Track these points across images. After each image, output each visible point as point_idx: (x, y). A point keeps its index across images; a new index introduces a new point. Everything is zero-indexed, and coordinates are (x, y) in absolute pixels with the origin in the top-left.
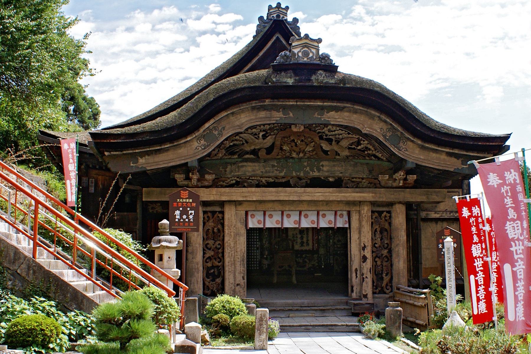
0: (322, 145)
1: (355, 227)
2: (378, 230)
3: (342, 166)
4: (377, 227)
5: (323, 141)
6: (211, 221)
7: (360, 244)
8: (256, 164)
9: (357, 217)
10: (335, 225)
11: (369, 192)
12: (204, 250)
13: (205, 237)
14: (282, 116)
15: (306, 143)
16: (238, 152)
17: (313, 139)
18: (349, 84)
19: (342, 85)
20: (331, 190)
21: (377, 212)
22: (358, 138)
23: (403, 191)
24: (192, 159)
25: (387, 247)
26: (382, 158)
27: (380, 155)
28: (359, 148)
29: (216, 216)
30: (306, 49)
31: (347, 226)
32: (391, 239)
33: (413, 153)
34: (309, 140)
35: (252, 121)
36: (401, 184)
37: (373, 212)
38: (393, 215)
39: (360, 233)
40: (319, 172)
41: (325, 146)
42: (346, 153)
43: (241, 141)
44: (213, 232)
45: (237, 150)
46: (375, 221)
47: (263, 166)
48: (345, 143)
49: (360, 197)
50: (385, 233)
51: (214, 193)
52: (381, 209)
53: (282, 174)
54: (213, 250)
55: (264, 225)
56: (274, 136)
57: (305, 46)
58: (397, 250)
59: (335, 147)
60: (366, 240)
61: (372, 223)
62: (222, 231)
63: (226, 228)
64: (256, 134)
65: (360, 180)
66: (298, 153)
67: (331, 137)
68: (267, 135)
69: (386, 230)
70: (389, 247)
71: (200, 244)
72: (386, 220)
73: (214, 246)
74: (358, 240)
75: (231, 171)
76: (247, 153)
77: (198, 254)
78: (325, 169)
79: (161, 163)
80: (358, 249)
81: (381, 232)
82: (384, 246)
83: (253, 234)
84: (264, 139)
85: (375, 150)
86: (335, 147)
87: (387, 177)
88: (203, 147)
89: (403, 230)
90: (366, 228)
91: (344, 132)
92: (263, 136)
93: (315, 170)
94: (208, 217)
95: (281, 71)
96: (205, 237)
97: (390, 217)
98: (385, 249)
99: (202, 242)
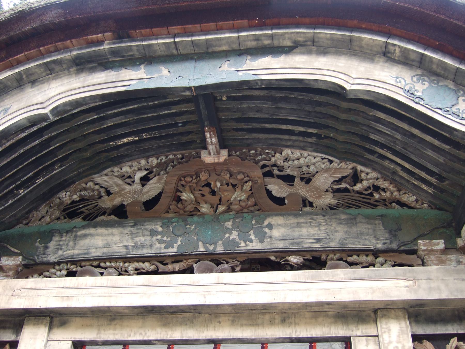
0: (271, 187)
3: (319, 225)
5: (272, 180)
8: (115, 231)
11: (397, 278)
16: (82, 212)
21: (431, 338)
34: (240, 176)
40: (262, 241)
41: (277, 189)
42: (329, 199)
45: (83, 209)
47: (132, 233)
48: (323, 181)
53: (173, 250)
59: (300, 189)
64: (130, 177)
65: (370, 259)
68: (151, 176)
75: (59, 248)
78: (276, 233)
84: (143, 185)
86: (300, 189)
87: (440, 244)
92: (142, 179)
93: (252, 237)
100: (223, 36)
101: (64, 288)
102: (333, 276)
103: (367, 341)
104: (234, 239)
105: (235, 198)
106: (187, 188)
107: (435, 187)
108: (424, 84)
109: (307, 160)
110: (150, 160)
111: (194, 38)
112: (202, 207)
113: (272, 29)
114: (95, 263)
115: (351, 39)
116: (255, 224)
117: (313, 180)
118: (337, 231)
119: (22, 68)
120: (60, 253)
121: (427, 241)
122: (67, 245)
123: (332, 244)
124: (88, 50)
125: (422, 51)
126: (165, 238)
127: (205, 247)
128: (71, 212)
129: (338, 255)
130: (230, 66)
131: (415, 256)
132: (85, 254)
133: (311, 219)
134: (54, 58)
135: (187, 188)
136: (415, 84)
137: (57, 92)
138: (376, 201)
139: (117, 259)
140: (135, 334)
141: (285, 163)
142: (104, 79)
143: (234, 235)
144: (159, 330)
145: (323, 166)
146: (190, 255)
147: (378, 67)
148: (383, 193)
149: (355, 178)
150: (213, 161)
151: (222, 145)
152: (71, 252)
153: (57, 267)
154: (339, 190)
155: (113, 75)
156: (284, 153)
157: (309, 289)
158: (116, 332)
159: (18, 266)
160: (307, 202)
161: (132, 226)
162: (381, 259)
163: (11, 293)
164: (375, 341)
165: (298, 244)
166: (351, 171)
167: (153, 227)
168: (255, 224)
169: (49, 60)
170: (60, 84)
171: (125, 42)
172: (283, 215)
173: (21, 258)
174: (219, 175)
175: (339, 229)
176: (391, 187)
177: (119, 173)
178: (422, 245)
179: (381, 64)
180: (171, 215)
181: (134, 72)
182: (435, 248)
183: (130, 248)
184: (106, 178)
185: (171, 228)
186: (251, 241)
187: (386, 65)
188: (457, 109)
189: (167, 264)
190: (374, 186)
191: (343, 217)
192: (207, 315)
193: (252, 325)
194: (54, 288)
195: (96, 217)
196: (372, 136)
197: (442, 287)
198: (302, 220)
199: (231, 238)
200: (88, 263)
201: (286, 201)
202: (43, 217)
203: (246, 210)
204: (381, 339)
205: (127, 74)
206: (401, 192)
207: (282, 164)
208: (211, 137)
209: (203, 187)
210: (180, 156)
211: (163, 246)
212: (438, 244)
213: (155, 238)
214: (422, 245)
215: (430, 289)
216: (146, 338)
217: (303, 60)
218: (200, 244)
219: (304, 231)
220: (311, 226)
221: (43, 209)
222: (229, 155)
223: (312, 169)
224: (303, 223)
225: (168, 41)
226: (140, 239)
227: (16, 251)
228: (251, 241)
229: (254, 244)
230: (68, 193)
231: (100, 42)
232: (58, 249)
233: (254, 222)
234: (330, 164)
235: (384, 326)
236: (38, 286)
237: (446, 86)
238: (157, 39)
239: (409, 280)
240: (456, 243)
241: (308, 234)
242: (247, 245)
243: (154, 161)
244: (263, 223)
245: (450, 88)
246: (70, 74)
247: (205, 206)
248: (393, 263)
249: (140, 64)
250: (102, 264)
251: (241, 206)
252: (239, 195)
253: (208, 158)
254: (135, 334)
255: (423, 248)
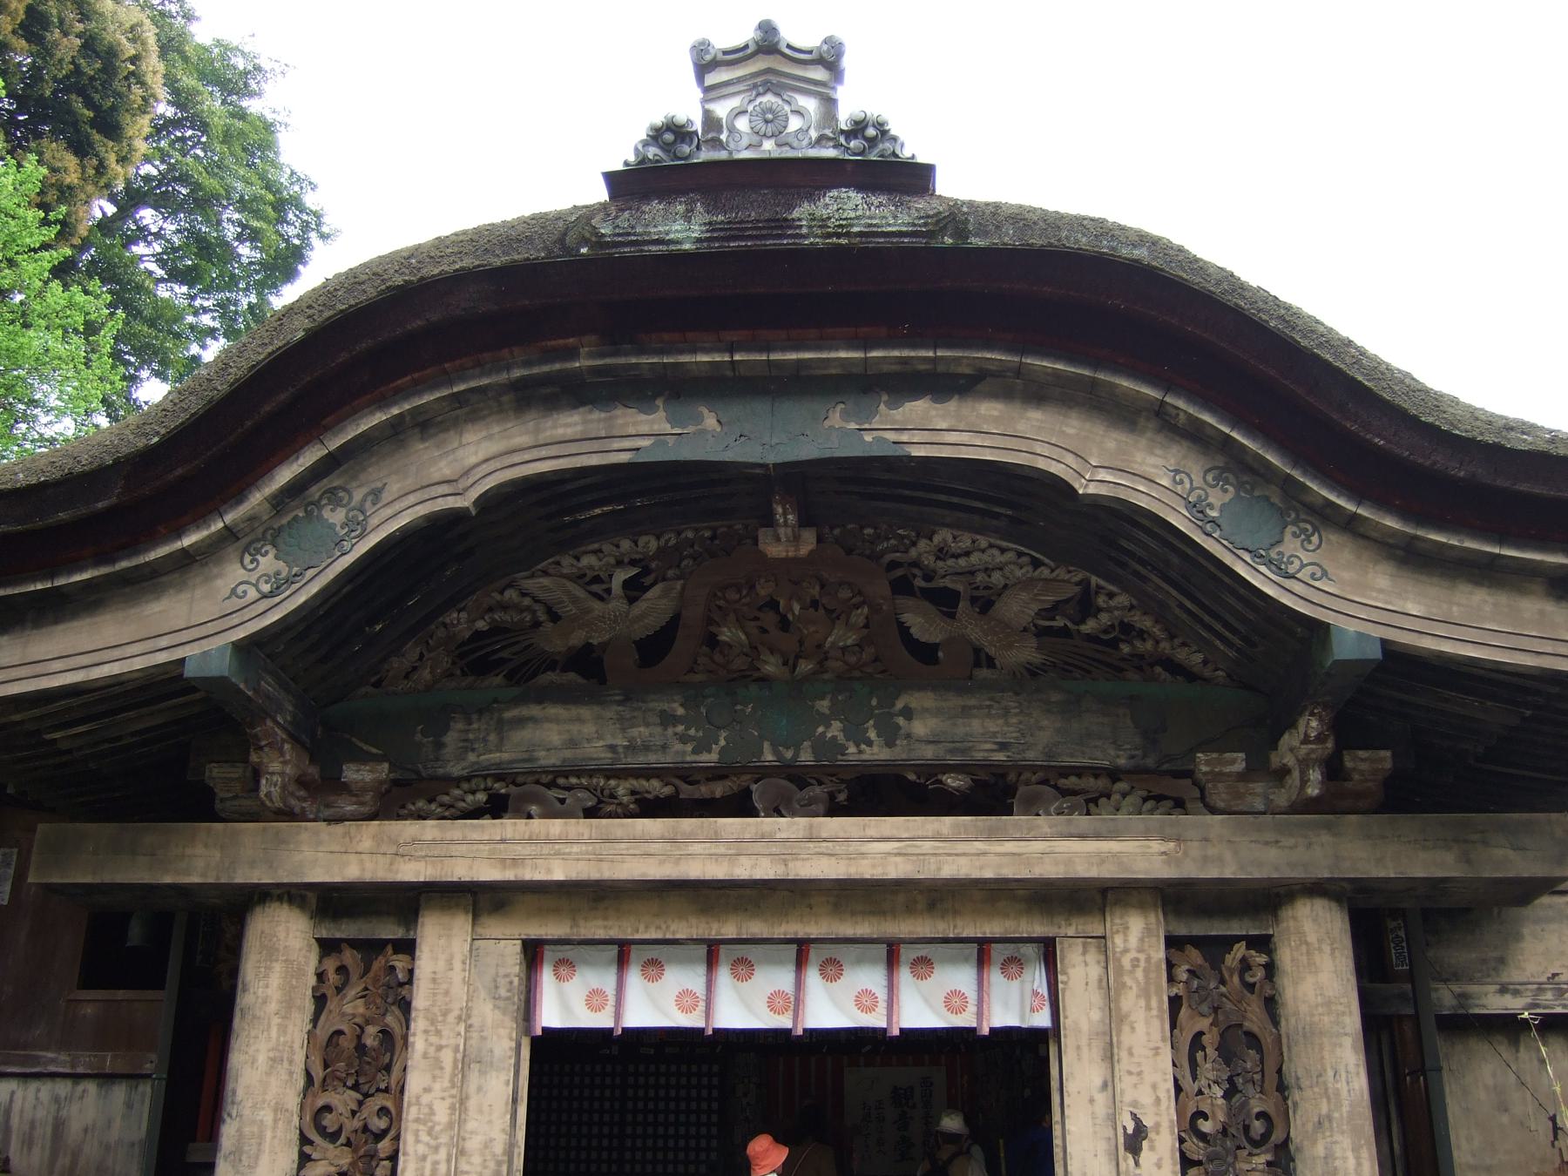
0: (909, 618)
1: (1085, 1026)
2: (1210, 1040)
3: (1006, 713)
4: (1204, 1024)
5: (910, 602)
6: (352, 992)
7: (1113, 1119)
8: (585, 712)
9: (1095, 971)
10: (980, 1015)
11: (1146, 835)
12: (304, 1140)
13: (318, 1073)
14: (667, 428)
15: (829, 611)
16: (503, 661)
17: (860, 593)
18: (984, 233)
19: (949, 241)
20: (946, 823)
21: (1197, 942)
22: (1085, 583)
23: (1328, 827)
24: (206, 645)
25: (1266, 1137)
26: (1207, 673)
27: (1198, 658)
28: (1089, 626)
29: (378, 964)
30: (768, 99)
31: (1042, 1020)
32: (1282, 1088)
33: (1357, 597)
34: (845, 594)
35: (517, 458)
36: (1313, 791)
37: (1172, 942)
38: (1286, 956)
39: (1110, 1057)
40: (890, 744)
41: (922, 623)
42: (1027, 653)
43: (528, 609)
44: (361, 1048)
45: (505, 654)
46: (1190, 992)
47: (621, 719)
48: (1018, 608)
49: (1102, 859)
50: (1251, 1059)
51: (367, 844)
52: (1217, 928)
53: (710, 758)
54: (348, 1144)
55: (618, 1015)
56: (679, 585)
57: (769, 88)
58: (1320, 1150)
59: (972, 628)
60: (1146, 1098)
61: (1175, 1003)
62: (393, 1044)
63: (419, 1024)
64: (597, 580)
65: (1102, 783)
66: (790, 663)
67: (947, 582)
68: (648, 580)
69: (1253, 1040)
70: (1277, 1137)
71: (278, 1109)
72: (1251, 987)
73: (358, 1123)
74: (1101, 1099)
75: (467, 746)
76: (552, 666)
77: (265, 1159)
78: (919, 728)
79: (57, 666)
80: (1102, 1146)
81: (1227, 1054)
82: (1247, 1128)
83: (560, 1063)
84: (632, 601)
85: (1172, 637)
86: (972, 628)
87: (1237, 762)
88: (266, 588)
89: (1348, 1042)
90: (1141, 1028)
91: (1010, 556)
92: (627, 584)
93: (872, 734)
94: (342, 970)
95: (646, 197)
96: (318, 1073)
97: (1271, 969)
98: (1257, 1144)
99: (293, 1102)
100: (833, 355)
101: (503, 841)
102: (1030, 830)
103: (1085, 946)
104: (834, 738)
105: (833, 643)
106: (732, 617)
107: (1238, 650)
108: (1226, 491)
109: (985, 557)
110: (642, 540)
111: (774, 356)
112: (766, 662)
113: (935, 348)
114: (546, 779)
115: (1094, 382)
116: (876, 707)
117: (997, 605)
118: (1041, 728)
119: (407, 407)
120: (472, 757)
121: (1215, 755)
122: (485, 740)
123: (1030, 755)
124: (546, 368)
125: (1226, 430)
126: (692, 732)
127: (775, 752)
128: (477, 658)
129: (1040, 775)
130: (846, 416)
131: (1188, 782)
132: (524, 761)
133: (991, 699)
134: (473, 384)
135: (732, 617)
136: (1209, 490)
137: (481, 457)
138: (1123, 659)
139: (591, 773)
140: (647, 927)
141: (940, 563)
142: (579, 428)
143: (835, 730)
144: (694, 921)
145: (1019, 573)
146: (744, 770)
147: (1143, 442)
148: (1138, 644)
149: (1085, 604)
150: (783, 555)
151: (805, 521)
152: (495, 757)
153: (465, 786)
154: (1049, 631)
155: (599, 420)
156: (937, 539)
157: (985, 854)
158: (610, 923)
159: (381, 782)
160: (983, 656)
161: (619, 703)
162: (1122, 786)
163: (393, 849)
164: (1099, 947)
165: (963, 751)
166: (1077, 589)
167: (666, 706)
168: (876, 707)
169: (462, 387)
170: (484, 433)
171: (626, 355)
172: (934, 689)
173: (386, 765)
174: (796, 583)
175: (1045, 723)
176: (1156, 630)
177: (575, 570)
178: (1204, 763)
179: (1149, 434)
180: (699, 677)
181: (643, 417)
182: (1227, 769)
183: (621, 750)
184: (545, 581)
185: (703, 710)
186: (870, 743)
187: (1160, 438)
188: (1279, 553)
189: (698, 782)
190: (1122, 623)
191: (1056, 697)
192: (786, 893)
193: (873, 913)
194: (481, 842)
195: (535, 675)
196: (1124, 543)
197: (1228, 855)
198: (972, 702)
199: (829, 735)
200: (530, 779)
201: (940, 654)
202: (415, 669)
203: (857, 674)
204: (1109, 944)
205: (630, 420)
206: (1177, 641)
207: (932, 565)
208: (785, 514)
209: (760, 609)
210: (707, 534)
211: (689, 748)
212: (1233, 762)
213: (670, 731)
214: (1204, 763)
215: (1205, 859)
216: (669, 936)
217: (996, 413)
218: (766, 745)
219: (976, 725)
220: (989, 716)
221: (412, 652)
222: (819, 540)
223: (997, 578)
224: (974, 707)
225: (717, 358)
226: (640, 732)
227: (374, 751)
228: (870, 743)
229: (875, 749)
230: (463, 615)
231: (572, 353)
232: (466, 750)
233: (874, 702)
234: (1035, 568)
235: (1117, 921)
236: (448, 836)
237: (1267, 498)
238: (694, 351)
239: (1170, 840)
240: (1268, 760)
241: (990, 733)
242: (860, 752)
243: (650, 544)
244: (893, 705)
245: (1273, 504)
246: (501, 410)
247: (772, 659)
248: (1145, 794)
249: (654, 397)
250: (561, 781)
251: (846, 663)
252: (842, 636)
253: (775, 548)
254: (647, 927)
255: (1204, 769)
